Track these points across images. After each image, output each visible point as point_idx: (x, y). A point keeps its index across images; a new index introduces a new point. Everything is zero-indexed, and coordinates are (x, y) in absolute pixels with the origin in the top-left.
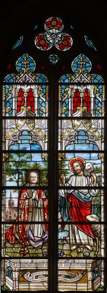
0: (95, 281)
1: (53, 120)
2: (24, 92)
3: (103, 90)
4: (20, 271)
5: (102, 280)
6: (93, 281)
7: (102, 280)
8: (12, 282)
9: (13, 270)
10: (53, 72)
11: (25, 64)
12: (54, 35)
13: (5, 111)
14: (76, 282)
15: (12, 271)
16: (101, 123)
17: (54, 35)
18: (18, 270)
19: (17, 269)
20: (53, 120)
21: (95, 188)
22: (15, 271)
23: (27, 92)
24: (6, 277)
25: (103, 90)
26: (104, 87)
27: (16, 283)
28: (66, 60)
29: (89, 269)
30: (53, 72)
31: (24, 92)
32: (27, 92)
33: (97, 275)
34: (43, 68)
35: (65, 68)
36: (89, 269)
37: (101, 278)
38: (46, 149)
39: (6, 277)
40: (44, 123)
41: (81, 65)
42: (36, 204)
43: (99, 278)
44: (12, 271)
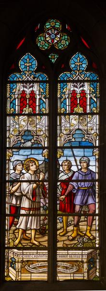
0: (91, 272)
1: (54, 115)
2: (77, 94)
3: (46, 90)
4: (22, 262)
5: (98, 270)
6: (88, 272)
7: (98, 270)
8: (15, 272)
9: (17, 260)
10: (53, 70)
11: (27, 63)
12: (52, 36)
13: (9, 109)
14: (74, 273)
15: (15, 262)
16: (96, 119)
17: (52, 36)
18: (21, 261)
19: (20, 260)
20: (54, 115)
21: (88, 181)
22: (18, 262)
23: (80, 94)
24: (10, 268)
25: (46, 90)
26: (48, 85)
27: (18, 274)
28: (65, 56)
29: (85, 260)
30: (53, 70)
31: (77, 94)
32: (80, 94)
33: (92, 266)
34: (44, 68)
35: (63, 64)
36: (85, 260)
37: (96, 269)
38: (46, 146)
39: (10, 268)
40: (45, 120)
41: (79, 61)
42: (40, 264)
43: (94, 269)
44: (15, 262)
